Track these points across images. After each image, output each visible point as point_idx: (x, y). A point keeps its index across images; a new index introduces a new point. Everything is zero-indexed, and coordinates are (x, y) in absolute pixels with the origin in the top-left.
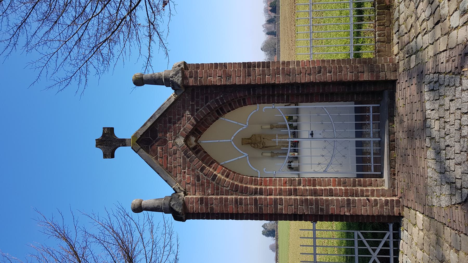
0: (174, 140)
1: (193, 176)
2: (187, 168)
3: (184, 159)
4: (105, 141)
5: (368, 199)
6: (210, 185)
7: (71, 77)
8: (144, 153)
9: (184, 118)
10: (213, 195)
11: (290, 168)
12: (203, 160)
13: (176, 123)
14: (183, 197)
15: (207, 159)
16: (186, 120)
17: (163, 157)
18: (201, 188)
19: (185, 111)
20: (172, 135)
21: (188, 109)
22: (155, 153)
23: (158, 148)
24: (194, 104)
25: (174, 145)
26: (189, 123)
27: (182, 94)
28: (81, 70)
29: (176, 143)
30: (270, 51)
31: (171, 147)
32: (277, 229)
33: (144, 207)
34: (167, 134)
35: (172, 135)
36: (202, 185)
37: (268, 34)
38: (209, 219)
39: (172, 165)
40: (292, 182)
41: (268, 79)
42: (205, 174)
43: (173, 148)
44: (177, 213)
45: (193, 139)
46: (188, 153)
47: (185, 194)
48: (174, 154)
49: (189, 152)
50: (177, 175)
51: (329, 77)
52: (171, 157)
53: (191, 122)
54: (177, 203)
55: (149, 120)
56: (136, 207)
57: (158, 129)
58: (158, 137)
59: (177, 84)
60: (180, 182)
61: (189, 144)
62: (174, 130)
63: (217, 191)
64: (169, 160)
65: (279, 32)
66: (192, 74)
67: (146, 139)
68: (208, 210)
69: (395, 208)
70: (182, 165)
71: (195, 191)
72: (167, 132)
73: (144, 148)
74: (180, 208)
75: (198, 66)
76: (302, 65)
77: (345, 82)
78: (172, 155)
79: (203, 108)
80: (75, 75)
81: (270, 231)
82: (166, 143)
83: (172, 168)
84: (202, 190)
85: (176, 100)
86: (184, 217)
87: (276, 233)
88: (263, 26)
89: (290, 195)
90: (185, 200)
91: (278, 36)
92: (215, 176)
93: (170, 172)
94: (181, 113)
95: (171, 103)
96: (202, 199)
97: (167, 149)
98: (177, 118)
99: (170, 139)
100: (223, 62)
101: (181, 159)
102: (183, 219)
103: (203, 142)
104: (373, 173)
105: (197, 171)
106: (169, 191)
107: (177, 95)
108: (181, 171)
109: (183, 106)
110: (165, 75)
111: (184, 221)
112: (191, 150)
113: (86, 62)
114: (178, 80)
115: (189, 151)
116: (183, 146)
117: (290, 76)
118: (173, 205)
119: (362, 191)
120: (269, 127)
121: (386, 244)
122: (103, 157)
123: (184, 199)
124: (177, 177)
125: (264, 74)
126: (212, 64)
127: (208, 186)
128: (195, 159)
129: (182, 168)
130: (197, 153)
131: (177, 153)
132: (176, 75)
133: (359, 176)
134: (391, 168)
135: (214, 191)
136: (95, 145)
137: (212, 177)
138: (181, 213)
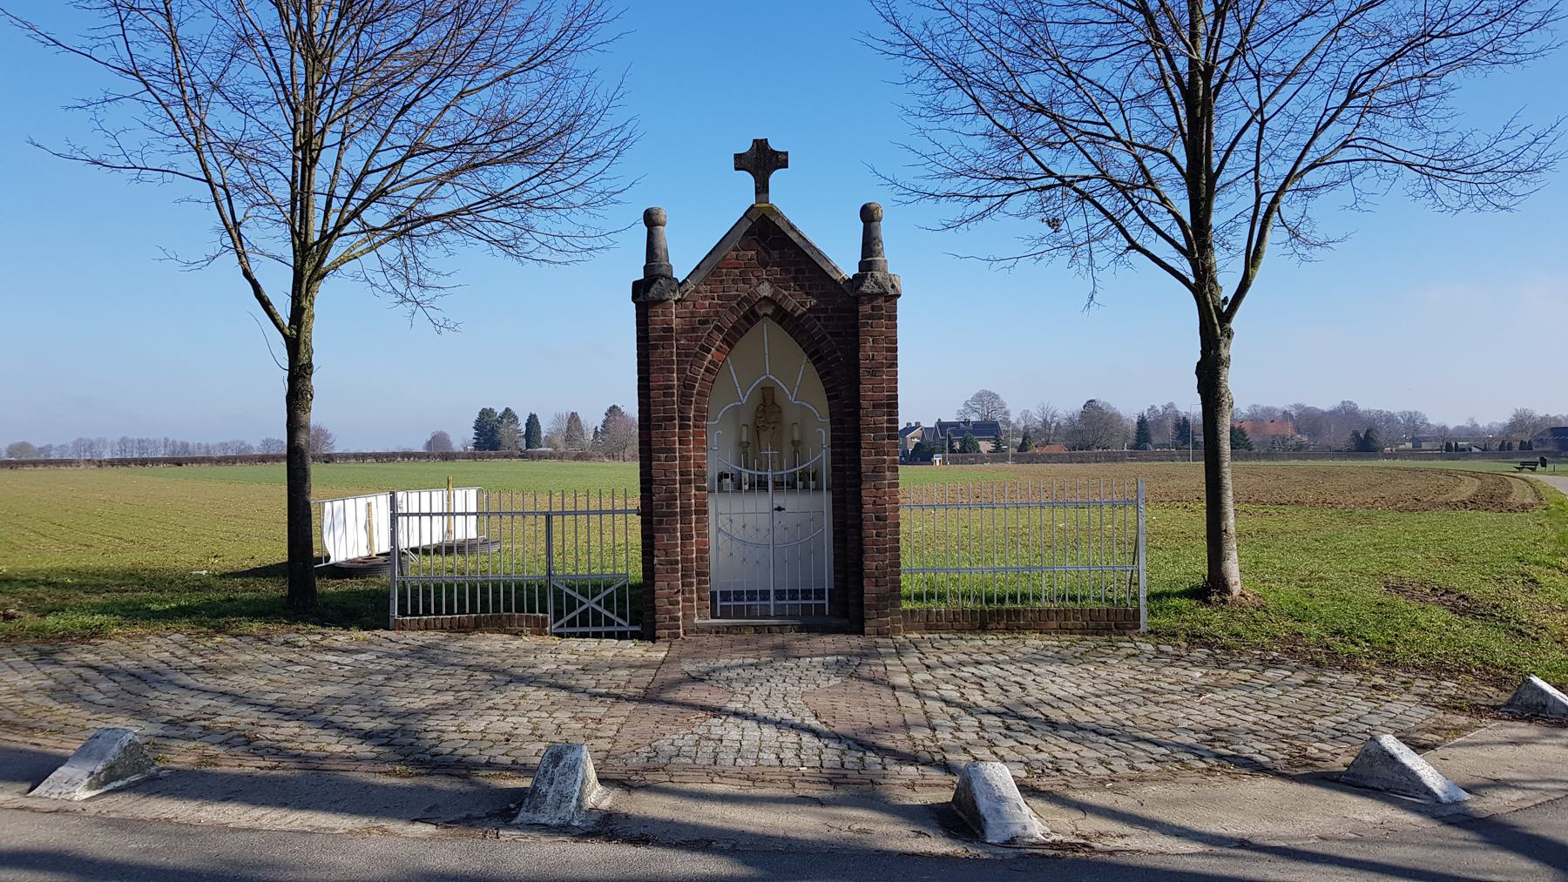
3: (736, 297)
4: (765, 156)
5: (679, 591)
10: (677, 348)
11: (722, 476)
12: (733, 328)
13: (795, 282)
30: (1080, 432)
32: (505, 457)
33: (655, 232)
36: (693, 330)
37: (1142, 422)
40: (701, 476)
41: (868, 437)
44: (647, 290)
51: (870, 532)
56: (654, 218)
59: (861, 285)
60: (697, 291)
63: (684, 354)
65: (1146, 460)
69: (667, 631)
75: (892, 317)
76: (891, 492)
77: (861, 557)
81: (493, 435)
86: (640, 299)
87: (493, 452)
88: (1171, 405)
89: (682, 474)
91: (1132, 457)
92: (709, 351)
100: (899, 362)
104: (719, 604)
106: (680, 273)
111: (634, 299)
114: (868, 287)
117: (873, 471)
118: (660, 283)
119: (691, 584)
120: (796, 437)
121: (609, 622)
125: (877, 430)
130: (745, 317)
132: (876, 283)
133: (713, 594)
134: (728, 628)
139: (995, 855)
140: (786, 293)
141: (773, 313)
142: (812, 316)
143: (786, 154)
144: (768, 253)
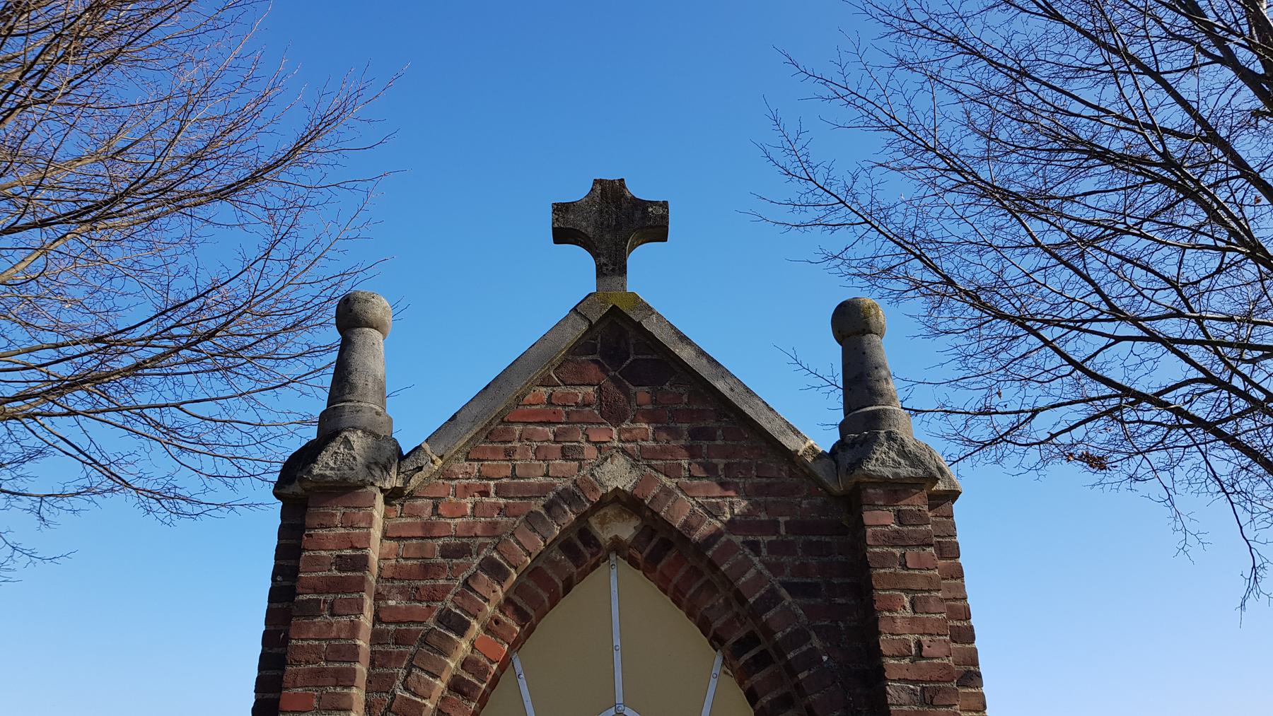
0: (624, 451)
1: (470, 527)
2: (502, 501)
3: (543, 490)
4: (619, 207)
6: (420, 602)
7: (811, 180)
9: (717, 491)
10: (377, 619)
12: (533, 572)
13: (692, 456)
15: (540, 590)
16: (707, 498)
17: (552, 408)
18: (409, 562)
19: (746, 496)
20: (643, 440)
21: (756, 505)
23: (590, 390)
24: (777, 532)
25: (600, 450)
26: (693, 512)
27: (819, 483)
31: (593, 439)
33: (355, 339)
34: (648, 423)
35: (645, 443)
39: (520, 440)
42: (470, 582)
43: (587, 445)
45: (626, 530)
47: (392, 496)
50: (474, 460)
52: (552, 437)
53: (702, 521)
54: (354, 458)
56: (357, 307)
62: (664, 451)
64: (541, 428)
66: (912, 522)
70: (518, 484)
71: (399, 538)
72: (657, 422)
74: (332, 469)
75: (950, 551)
78: (558, 442)
79: (766, 572)
80: (820, 191)
83: (505, 442)
84: (402, 567)
85: (789, 456)
86: (295, 488)
90: (365, 490)
93: (491, 433)
95: (776, 435)
96: (361, 563)
97: (584, 423)
98: (715, 461)
99: (627, 435)
102: (287, 486)
105: (488, 544)
107: (815, 459)
109: (768, 485)
113: (866, 222)
115: (574, 510)
118: (347, 442)
123: (370, 488)
124: (466, 464)
126: (968, 617)
127: (412, 595)
129: (505, 480)
130: (565, 545)
131: (566, 460)
135: (392, 619)
137: (458, 611)
138: (310, 472)
139: (619, 385)
140: (669, 483)
141: (636, 538)
142: (737, 539)
144: (627, 393)
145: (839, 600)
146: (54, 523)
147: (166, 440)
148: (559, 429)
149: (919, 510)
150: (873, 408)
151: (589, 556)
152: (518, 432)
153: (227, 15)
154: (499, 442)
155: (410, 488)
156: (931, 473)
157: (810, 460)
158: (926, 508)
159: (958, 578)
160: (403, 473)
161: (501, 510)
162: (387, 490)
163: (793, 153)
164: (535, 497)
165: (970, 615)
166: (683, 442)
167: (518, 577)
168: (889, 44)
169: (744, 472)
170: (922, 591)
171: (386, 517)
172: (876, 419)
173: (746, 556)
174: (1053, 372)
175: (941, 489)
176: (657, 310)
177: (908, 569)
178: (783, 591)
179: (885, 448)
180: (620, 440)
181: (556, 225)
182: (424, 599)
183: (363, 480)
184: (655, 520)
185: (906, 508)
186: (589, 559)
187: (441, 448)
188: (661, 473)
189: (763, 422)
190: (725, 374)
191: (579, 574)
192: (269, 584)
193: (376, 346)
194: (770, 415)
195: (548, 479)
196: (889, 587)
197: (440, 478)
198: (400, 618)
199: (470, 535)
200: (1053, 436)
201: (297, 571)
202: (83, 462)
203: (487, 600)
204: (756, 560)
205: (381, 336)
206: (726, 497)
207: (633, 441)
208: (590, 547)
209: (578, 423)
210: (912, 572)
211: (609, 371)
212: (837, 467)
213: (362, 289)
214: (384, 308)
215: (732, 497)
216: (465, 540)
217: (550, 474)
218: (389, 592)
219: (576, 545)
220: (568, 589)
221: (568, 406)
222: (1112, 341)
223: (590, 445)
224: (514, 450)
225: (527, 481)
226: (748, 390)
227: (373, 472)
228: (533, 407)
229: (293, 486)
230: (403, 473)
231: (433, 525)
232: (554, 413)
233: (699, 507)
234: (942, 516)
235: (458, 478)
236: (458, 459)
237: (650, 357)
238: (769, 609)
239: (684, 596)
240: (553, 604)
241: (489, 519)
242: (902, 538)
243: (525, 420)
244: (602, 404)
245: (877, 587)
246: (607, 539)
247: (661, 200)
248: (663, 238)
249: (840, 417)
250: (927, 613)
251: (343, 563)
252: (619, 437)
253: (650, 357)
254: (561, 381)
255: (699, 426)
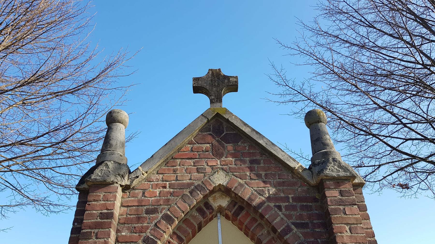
0: (222, 169)
1: (158, 201)
2: (172, 190)
3: (189, 185)
4: (219, 79)
6: (136, 233)
7: (287, 85)
8: (200, 125)
9: (262, 185)
12: (185, 221)
13: (251, 171)
14: (119, 183)
15: (188, 228)
16: (258, 187)
17: (193, 153)
18: (132, 216)
19: (275, 186)
20: (230, 165)
21: (279, 190)
22: (199, 140)
23: (208, 145)
24: (288, 201)
25: (212, 169)
26: (253, 194)
27: (305, 181)
28: (297, 94)
29: (217, 171)
31: (209, 164)
34: (232, 158)
35: (231, 166)
36: (139, 219)
38: (72, 233)
39: (179, 166)
42: (158, 224)
43: (207, 167)
45: (224, 202)
46: (199, 192)
47: (125, 188)
48: (197, 168)
49: (200, 193)
50: (160, 174)
52: (193, 164)
53: (256, 197)
54: (109, 172)
55: (254, 130)
56: (114, 115)
57: (239, 144)
58: (226, 145)
60: (148, 180)
61: (215, 196)
62: (239, 168)
64: (188, 161)
66: (347, 195)
67: (223, 128)
68: (87, 228)
70: (178, 183)
71: (128, 206)
72: (236, 158)
73: (207, 125)
74: (100, 176)
78: (195, 166)
79: (285, 219)
80: (291, 89)
82: (216, 156)
83: (173, 166)
84: (129, 218)
85: (291, 170)
86: (85, 186)
90: (113, 185)
93: (167, 163)
94: (269, 180)
95: (286, 161)
96: (110, 216)
97: (206, 158)
98: (260, 172)
99: (224, 163)
101: (190, 180)
102: (81, 185)
103: (219, 225)
105: (165, 208)
107: (303, 171)
108: (168, 181)
109: (283, 182)
110: (333, 153)
112: (203, 197)
113: (309, 99)
115: (202, 193)
116: (212, 184)
118: (107, 165)
122: (195, 77)
123: (115, 184)
124: (157, 175)
126: (374, 236)
127: (133, 230)
128: (187, 205)
129: (173, 182)
130: (200, 210)
131: (199, 173)
135: (123, 241)
136: (212, 69)
137: (152, 237)
138: (90, 178)
141: (228, 206)
142: (272, 205)
143: (236, 77)
144: (223, 147)
145: (317, 230)
146: (8, 217)
147: (45, 181)
148: (195, 161)
149: (349, 190)
150: (325, 150)
151: (208, 213)
152: (178, 163)
153: (77, 31)
154: (171, 166)
155: (133, 185)
156: (353, 174)
157: (301, 171)
158: (352, 189)
159: (368, 219)
160: (130, 179)
161: (171, 194)
162: (123, 186)
163: (280, 76)
164: (186, 188)
165: (374, 235)
166: (247, 165)
167: (178, 223)
168: (314, 38)
169: (273, 177)
170: (354, 224)
171: (122, 197)
172: (327, 155)
173: (276, 211)
174: (382, 154)
175: (357, 182)
176: (234, 114)
177: (347, 215)
178: (293, 227)
179: (332, 165)
180: (221, 165)
181: (194, 85)
182: (137, 232)
183: (113, 181)
184: (236, 198)
185: (344, 189)
186: (208, 215)
187: (146, 169)
188: (238, 178)
189: (280, 156)
190: (263, 137)
191: (204, 222)
192: (71, 226)
193: (122, 130)
194: (283, 154)
195: (191, 181)
196: (339, 223)
197: (146, 181)
198: (127, 240)
199: (158, 204)
200: (385, 177)
201: (83, 220)
202: (12, 189)
203: (165, 232)
204: (280, 213)
205: (124, 127)
206: (266, 187)
207: (226, 165)
208: (209, 210)
209: (203, 158)
210: (349, 216)
211: (216, 138)
212: (312, 174)
213: (115, 108)
214: (125, 116)
215: (269, 187)
216: (156, 207)
217: (192, 179)
218: (123, 229)
219: (203, 209)
220: (200, 229)
221: (199, 152)
222: (405, 141)
223: (209, 167)
224: (177, 169)
225: (182, 182)
226: (273, 144)
227: (117, 178)
228: (185, 152)
229: (84, 185)
230: (130, 179)
231: (142, 200)
232: (194, 154)
233: (255, 191)
234: (358, 194)
235: (154, 181)
236: (154, 174)
237: (232, 132)
238: (287, 234)
239: (249, 230)
240: (194, 235)
241: (166, 198)
242: (343, 202)
243: (182, 157)
244: (213, 151)
245: (334, 223)
246: (216, 207)
247: (235, 76)
248: (236, 90)
249: (311, 156)
250: (357, 234)
251: (103, 216)
252: (221, 163)
253: (232, 132)
254: (197, 142)
255: (253, 159)
